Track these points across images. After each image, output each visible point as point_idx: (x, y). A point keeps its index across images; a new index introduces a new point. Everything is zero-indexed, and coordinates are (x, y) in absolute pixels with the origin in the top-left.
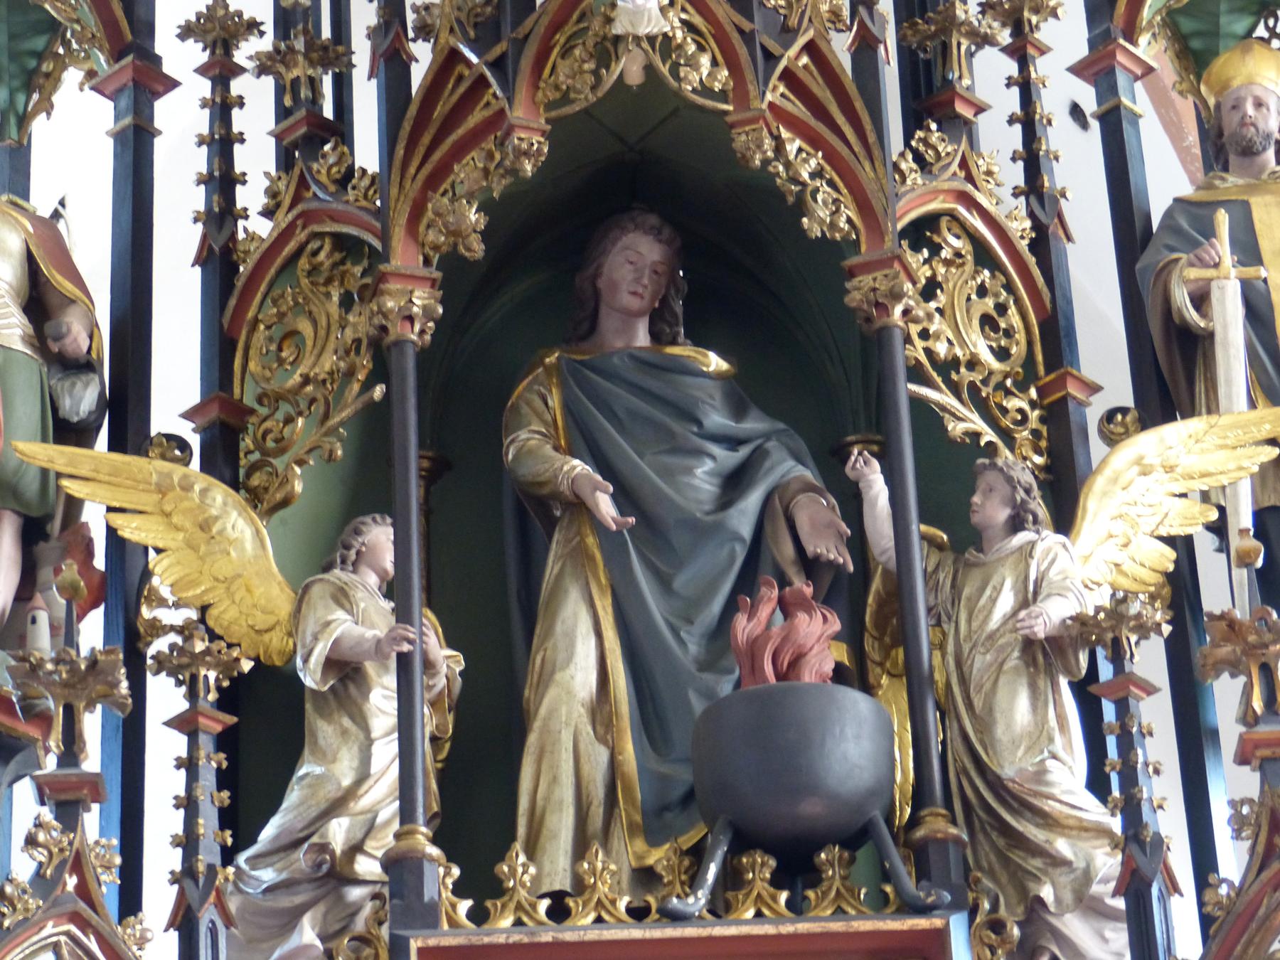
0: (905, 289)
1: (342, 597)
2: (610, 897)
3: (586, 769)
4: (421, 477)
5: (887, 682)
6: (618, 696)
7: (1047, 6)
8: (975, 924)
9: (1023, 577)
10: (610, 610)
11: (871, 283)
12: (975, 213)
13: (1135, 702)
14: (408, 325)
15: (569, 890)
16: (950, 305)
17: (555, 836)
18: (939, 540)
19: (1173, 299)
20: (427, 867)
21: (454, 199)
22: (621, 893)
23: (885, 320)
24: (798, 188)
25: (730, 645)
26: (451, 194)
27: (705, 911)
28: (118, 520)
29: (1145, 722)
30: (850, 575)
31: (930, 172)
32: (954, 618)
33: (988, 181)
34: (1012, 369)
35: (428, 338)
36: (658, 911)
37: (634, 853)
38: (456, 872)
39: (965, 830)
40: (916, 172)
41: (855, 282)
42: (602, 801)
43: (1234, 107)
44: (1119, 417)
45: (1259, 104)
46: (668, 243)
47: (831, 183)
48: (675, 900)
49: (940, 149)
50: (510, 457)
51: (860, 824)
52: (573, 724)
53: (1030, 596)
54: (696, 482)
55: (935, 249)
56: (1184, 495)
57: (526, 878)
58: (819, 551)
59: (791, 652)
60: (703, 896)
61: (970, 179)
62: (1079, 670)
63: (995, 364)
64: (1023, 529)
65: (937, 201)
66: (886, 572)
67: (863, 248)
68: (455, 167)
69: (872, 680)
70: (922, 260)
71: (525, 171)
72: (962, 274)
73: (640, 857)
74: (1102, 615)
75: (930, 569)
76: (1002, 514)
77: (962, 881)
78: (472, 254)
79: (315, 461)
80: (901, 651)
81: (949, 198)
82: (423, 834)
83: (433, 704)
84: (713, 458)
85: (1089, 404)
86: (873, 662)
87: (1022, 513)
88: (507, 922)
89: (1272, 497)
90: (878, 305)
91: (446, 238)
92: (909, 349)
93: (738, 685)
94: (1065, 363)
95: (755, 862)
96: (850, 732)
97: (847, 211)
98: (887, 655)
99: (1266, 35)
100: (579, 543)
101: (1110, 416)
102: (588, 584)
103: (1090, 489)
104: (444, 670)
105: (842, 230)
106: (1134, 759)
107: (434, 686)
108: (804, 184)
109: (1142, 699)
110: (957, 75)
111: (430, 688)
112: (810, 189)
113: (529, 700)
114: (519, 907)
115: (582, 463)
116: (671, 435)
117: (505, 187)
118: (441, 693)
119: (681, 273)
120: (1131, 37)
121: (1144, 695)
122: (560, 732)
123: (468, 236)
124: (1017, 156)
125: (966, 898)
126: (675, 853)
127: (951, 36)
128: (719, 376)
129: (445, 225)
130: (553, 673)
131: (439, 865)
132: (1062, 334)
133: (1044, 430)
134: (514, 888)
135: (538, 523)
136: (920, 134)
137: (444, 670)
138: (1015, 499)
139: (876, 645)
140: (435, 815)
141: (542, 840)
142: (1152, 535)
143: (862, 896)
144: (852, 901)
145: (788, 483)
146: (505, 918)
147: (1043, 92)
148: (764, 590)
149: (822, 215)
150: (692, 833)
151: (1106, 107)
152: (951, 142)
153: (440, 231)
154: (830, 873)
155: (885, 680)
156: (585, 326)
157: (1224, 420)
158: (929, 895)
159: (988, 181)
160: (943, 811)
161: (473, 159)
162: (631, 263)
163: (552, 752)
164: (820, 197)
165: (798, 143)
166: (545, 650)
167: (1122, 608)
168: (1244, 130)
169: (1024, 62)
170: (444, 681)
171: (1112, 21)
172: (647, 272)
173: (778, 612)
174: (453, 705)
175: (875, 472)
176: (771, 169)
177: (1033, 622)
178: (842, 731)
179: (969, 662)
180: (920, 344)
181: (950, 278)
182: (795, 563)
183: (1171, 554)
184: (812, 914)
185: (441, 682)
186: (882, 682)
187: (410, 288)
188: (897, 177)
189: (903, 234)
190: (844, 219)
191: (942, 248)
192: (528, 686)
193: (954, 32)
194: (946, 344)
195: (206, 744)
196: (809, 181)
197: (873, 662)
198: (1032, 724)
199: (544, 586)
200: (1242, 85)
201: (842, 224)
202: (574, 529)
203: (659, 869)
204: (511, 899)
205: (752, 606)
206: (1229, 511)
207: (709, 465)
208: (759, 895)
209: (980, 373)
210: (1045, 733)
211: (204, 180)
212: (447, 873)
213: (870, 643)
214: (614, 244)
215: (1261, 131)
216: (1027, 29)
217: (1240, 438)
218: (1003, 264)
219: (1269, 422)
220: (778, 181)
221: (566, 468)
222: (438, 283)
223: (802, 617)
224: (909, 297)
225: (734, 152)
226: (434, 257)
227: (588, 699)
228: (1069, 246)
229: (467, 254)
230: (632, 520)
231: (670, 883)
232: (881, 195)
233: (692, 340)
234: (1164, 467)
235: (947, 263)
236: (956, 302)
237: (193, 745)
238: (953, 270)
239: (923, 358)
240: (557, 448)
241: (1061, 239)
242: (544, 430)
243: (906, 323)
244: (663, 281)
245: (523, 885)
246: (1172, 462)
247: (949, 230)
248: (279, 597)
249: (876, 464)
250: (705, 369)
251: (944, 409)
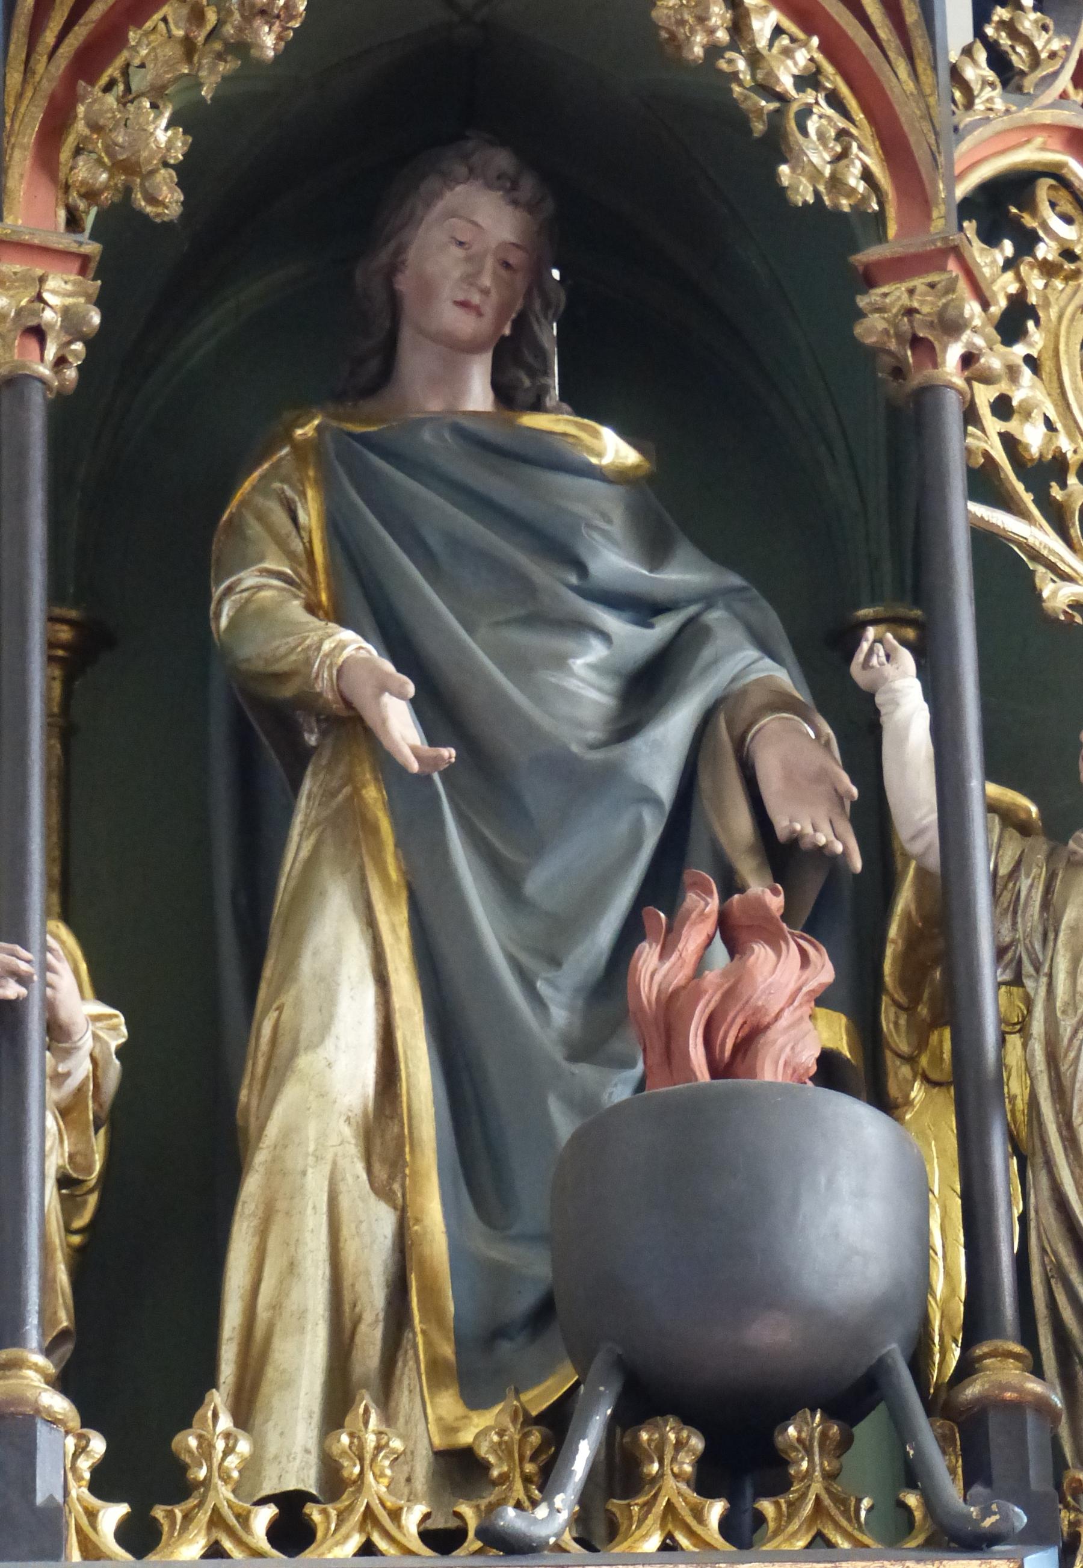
0: (967, 313)
2: (388, 1504)
3: (350, 1249)
4: (51, 659)
5: (922, 1094)
6: (416, 1106)
8: (351, 441)
10: (404, 932)
11: (905, 300)
14: (33, 345)
15: (313, 1491)
16: (1050, 353)
17: (288, 1384)
18: (1023, 816)
20: (43, 1434)
21: (128, 97)
22: (412, 1499)
23: (929, 371)
24: (773, 106)
25: (627, 1011)
26: (121, 87)
27: (567, 1537)
30: (856, 877)
31: (1019, 89)
32: (1046, 969)
35: (71, 374)
36: (480, 1534)
37: (439, 1419)
38: (98, 1445)
39: (1059, 1389)
40: (992, 85)
41: (875, 295)
42: (381, 1316)
46: (531, 208)
47: (834, 100)
48: (511, 1512)
49: (1039, 44)
50: (224, 622)
51: (862, 1371)
52: (329, 1157)
54: (572, 684)
55: (1027, 241)
57: (232, 1462)
58: (798, 827)
59: (739, 1021)
60: (565, 1501)
65: (1030, 146)
66: (922, 873)
67: (892, 230)
68: (131, 34)
69: (893, 1090)
70: (1001, 262)
71: (262, 47)
73: (450, 1430)
75: (1003, 871)
77: (1050, 1488)
78: (160, 210)
80: (947, 1033)
81: (1055, 142)
82: (37, 1368)
83: (65, 1112)
84: (605, 636)
86: (899, 1056)
90: (916, 342)
91: (111, 177)
92: (975, 441)
93: (641, 1087)
95: (663, 1439)
96: (845, 1182)
97: (862, 155)
98: (922, 1044)
100: (350, 799)
102: (363, 880)
104: (87, 1044)
105: (853, 190)
107: (68, 1075)
108: (783, 98)
111: (59, 1079)
112: (795, 107)
113: (248, 1104)
114: (217, 1520)
115: (359, 638)
116: (527, 588)
117: (224, 79)
118: (80, 1090)
119: (556, 274)
122: (304, 1173)
123: (153, 172)
125: (1056, 1520)
126: (514, 1420)
128: (619, 477)
129: (109, 149)
130: (294, 1054)
131: (67, 1433)
134: (207, 1482)
135: (272, 754)
136: (1001, 13)
137: (87, 1044)
139: (902, 1021)
140: (64, 1334)
141: (265, 1389)
143: (863, 1514)
144: (844, 1523)
145: (744, 692)
146: (191, 1541)
148: (692, 898)
149: (815, 159)
150: (549, 1382)
152: (1058, 33)
153: (99, 161)
154: (805, 1465)
155: (917, 1092)
156: (373, 365)
158: (986, 1513)
160: (1018, 1349)
161: (165, 20)
162: (461, 244)
163: (288, 1214)
164: (812, 125)
165: (775, 16)
166: (280, 1009)
170: (88, 1066)
172: (489, 263)
173: (719, 948)
174: (104, 1115)
175: (905, 675)
176: (722, 65)
178: (830, 1181)
179: (1072, 1055)
180: (994, 426)
181: (1052, 299)
182: (752, 850)
184: (768, 1547)
185: (80, 1068)
186: (913, 1095)
187: (39, 272)
188: (958, 95)
189: (967, 208)
190: (856, 170)
191: (1039, 239)
192: (246, 1081)
194: (1042, 429)
196: (793, 93)
197: (899, 1056)
199: (283, 882)
201: (854, 179)
202: (342, 769)
203: (483, 1451)
204: (200, 1505)
205: (669, 929)
207: (597, 651)
208: (670, 1506)
212: (81, 1450)
213: (892, 1017)
214: (428, 205)
220: (737, 89)
221: (327, 646)
222: (93, 265)
223: (761, 954)
224: (975, 330)
225: (656, 27)
226: (87, 213)
227: (358, 1110)
229: (149, 209)
230: (449, 753)
231: (504, 1478)
232: (926, 126)
233: (570, 404)
235: (1048, 269)
236: (1062, 340)
238: (1058, 284)
239: (999, 455)
240: (312, 608)
242: (289, 571)
243: (968, 381)
244: (520, 282)
245: (226, 1478)
247: (1053, 205)
249: (907, 660)
250: (594, 460)
251: (1036, 556)
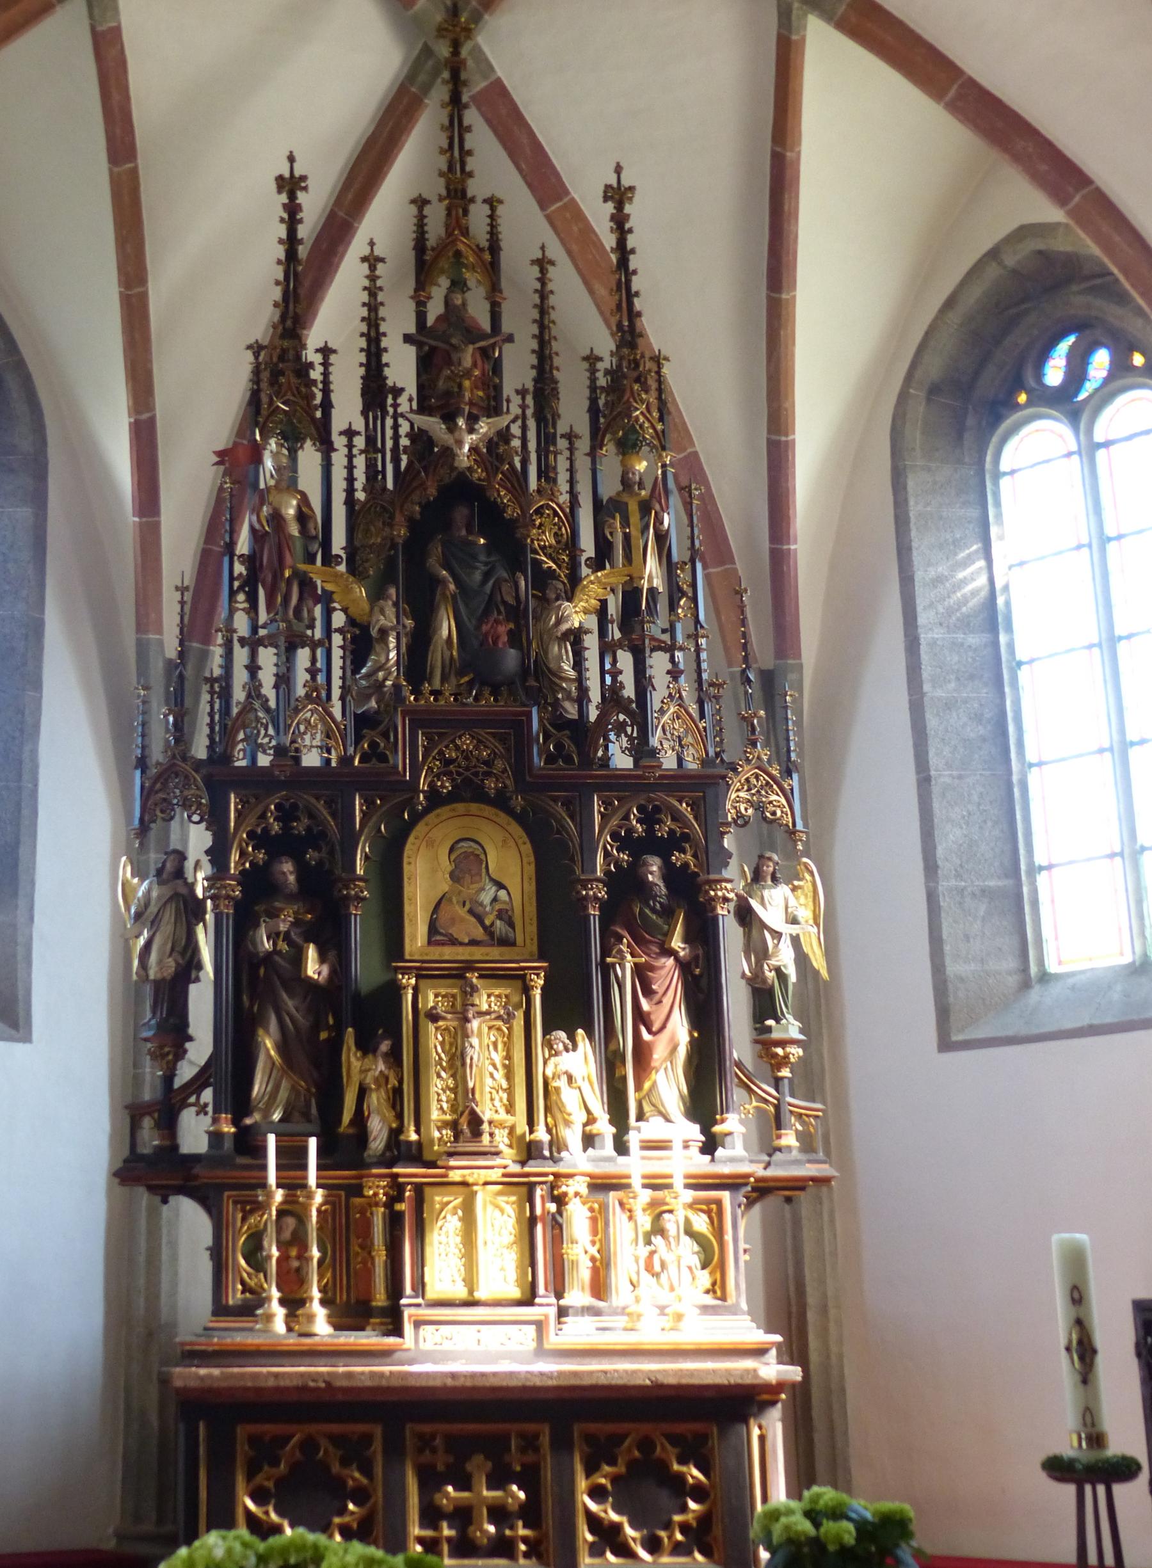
1: (382, 612)
28: (325, 584)
76: (553, 596)
79: (374, 572)
88: (423, 702)
101: (588, 559)
195: (348, 653)
211: (346, 479)
237: (344, 653)
248: (366, 606)
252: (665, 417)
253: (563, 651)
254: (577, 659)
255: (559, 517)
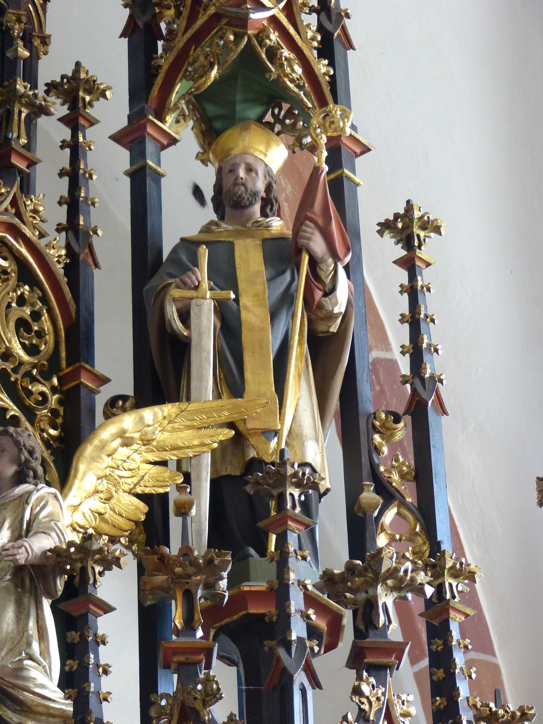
7: (98, 89)
9: (19, 518)
12: (21, 241)
13: (94, 617)
19: (166, 314)
29: (100, 633)
33: (35, 218)
34: (39, 361)
43: (231, 171)
44: (121, 403)
45: (250, 169)
53: (23, 533)
56: (164, 463)
61: (18, 215)
62: (56, 592)
63: (25, 357)
64: (26, 482)
72: (6, 287)
74: (72, 550)
85: (99, 392)
87: (26, 470)
89: (229, 467)
94: (81, 359)
99: (272, 120)
101: (112, 403)
103: (82, 454)
106: (86, 661)
109: (100, 616)
110: (15, 135)
120: (161, 117)
121: (102, 613)
124: (63, 201)
127: (14, 106)
132: (82, 337)
133: (61, 411)
138: (20, 459)
142: (129, 493)
147: (89, 153)
151: (136, 166)
157: (192, 406)
159: (35, 218)
167: (88, 544)
168: (237, 188)
169: (75, 128)
171: (147, 103)
177: (15, 551)
183: (143, 507)
193: (16, 103)
198: (16, 630)
200: (238, 154)
206: (193, 476)
209: (13, 363)
210: (24, 640)
215: (249, 190)
216: (81, 105)
217: (204, 421)
218: (41, 281)
219: (228, 410)
228: (96, 271)
234: (142, 440)
241: (90, 265)
246: (149, 437)
252: (338, 48)
253: (32, 624)
254: (73, 636)
255: (34, 282)
